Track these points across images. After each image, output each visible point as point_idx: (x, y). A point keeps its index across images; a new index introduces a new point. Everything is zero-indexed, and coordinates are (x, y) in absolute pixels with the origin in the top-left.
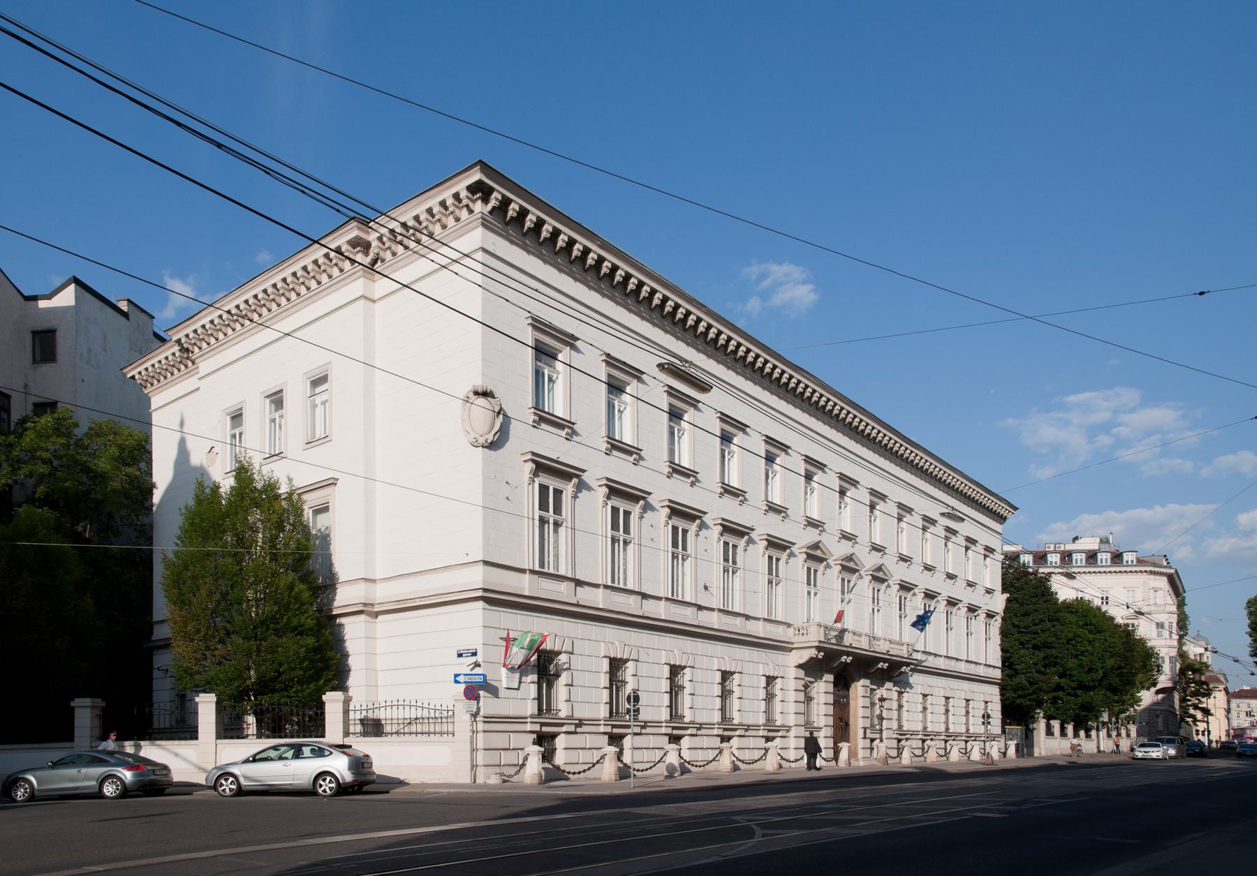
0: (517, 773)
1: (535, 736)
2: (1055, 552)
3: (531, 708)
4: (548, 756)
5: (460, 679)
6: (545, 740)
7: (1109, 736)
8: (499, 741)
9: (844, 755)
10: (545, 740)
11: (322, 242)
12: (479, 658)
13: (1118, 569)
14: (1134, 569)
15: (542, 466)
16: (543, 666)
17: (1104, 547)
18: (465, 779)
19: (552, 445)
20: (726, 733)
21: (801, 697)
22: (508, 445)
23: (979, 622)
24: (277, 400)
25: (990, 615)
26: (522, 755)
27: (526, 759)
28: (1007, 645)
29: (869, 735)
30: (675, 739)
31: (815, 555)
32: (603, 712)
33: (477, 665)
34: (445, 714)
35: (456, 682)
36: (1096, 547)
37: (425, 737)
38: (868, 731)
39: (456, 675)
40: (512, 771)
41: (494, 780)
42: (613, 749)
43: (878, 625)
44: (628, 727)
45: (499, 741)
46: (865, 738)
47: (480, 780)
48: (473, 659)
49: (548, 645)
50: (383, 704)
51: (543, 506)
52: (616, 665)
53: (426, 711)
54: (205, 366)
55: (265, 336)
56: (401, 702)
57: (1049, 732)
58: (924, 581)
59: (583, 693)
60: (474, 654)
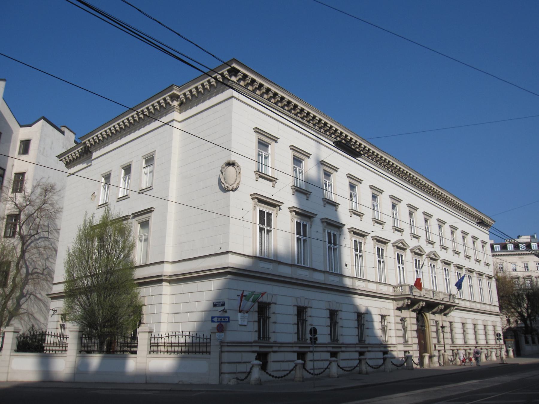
0: (246, 378)
1: (256, 354)
2: (510, 243)
3: (254, 337)
4: (264, 367)
5: (214, 319)
6: (262, 357)
7: (314, 331)
8: (235, 357)
9: (426, 360)
10: (262, 357)
11: (203, 74)
12: (226, 307)
13: (505, 253)
14: (500, 253)
15: (261, 200)
16: (263, 310)
17: (533, 240)
18: (214, 380)
19: (265, 189)
20: (362, 350)
21: (400, 326)
22: (223, 193)
23: (485, 281)
24: (127, 169)
25: (490, 278)
26: (249, 366)
27: (251, 369)
28: (501, 294)
29: (437, 348)
30: (334, 354)
31: (401, 247)
32: (293, 338)
33: (224, 311)
34: (205, 340)
35: (213, 321)
36: (529, 240)
37: (200, 355)
38: (437, 346)
39: (213, 318)
40: (243, 376)
41: (233, 382)
42: (300, 361)
43: (437, 283)
44: (309, 347)
45: (235, 357)
46: (435, 349)
47: (225, 382)
48: (222, 308)
49: (264, 299)
50: (163, 336)
51: (262, 222)
52: (301, 311)
53: (198, 339)
54: (95, 155)
55: (157, 124)
56: (181, 333)
57: (527, 342)
58: (460, 260)
59: (284, 329)
60: (223, 305)
